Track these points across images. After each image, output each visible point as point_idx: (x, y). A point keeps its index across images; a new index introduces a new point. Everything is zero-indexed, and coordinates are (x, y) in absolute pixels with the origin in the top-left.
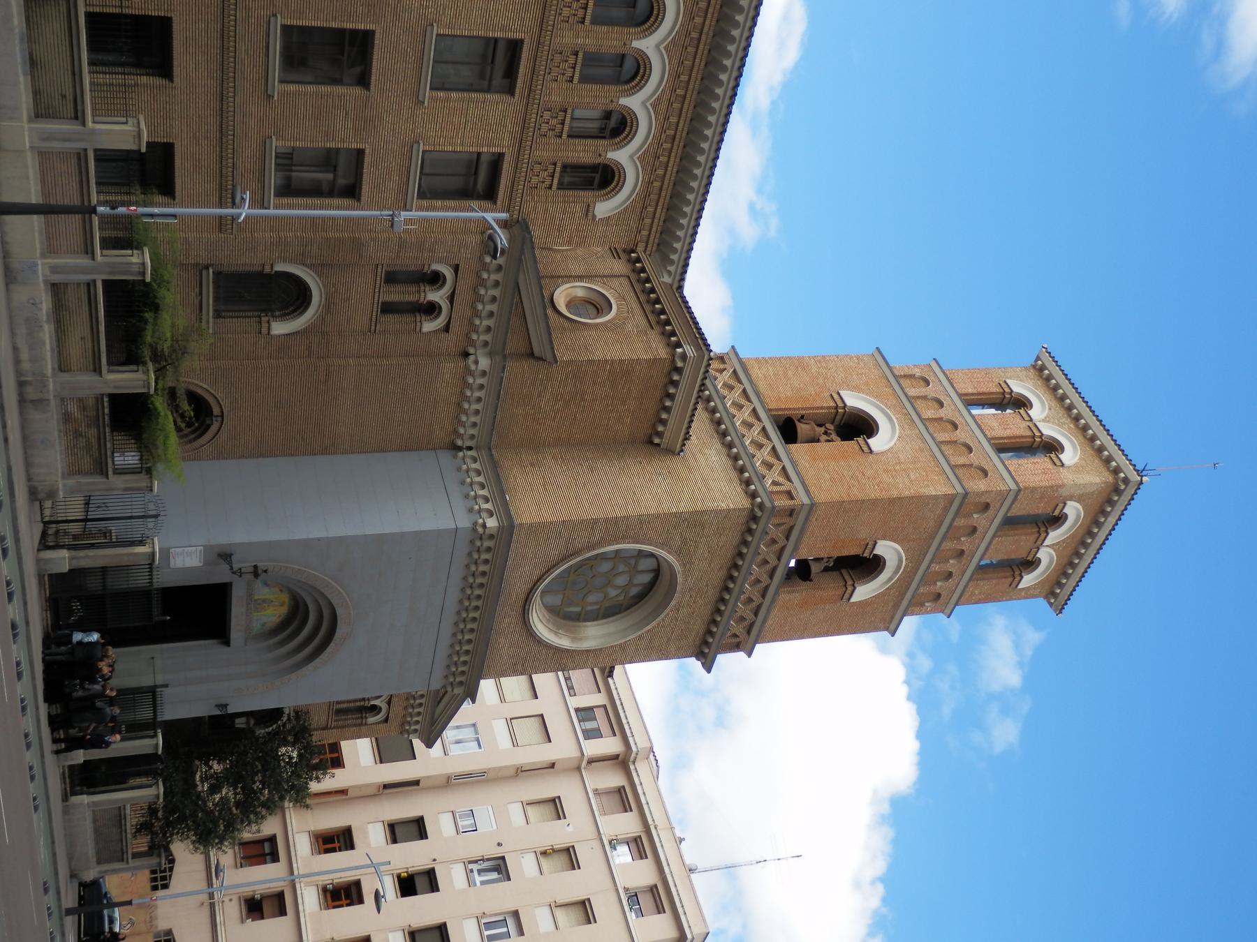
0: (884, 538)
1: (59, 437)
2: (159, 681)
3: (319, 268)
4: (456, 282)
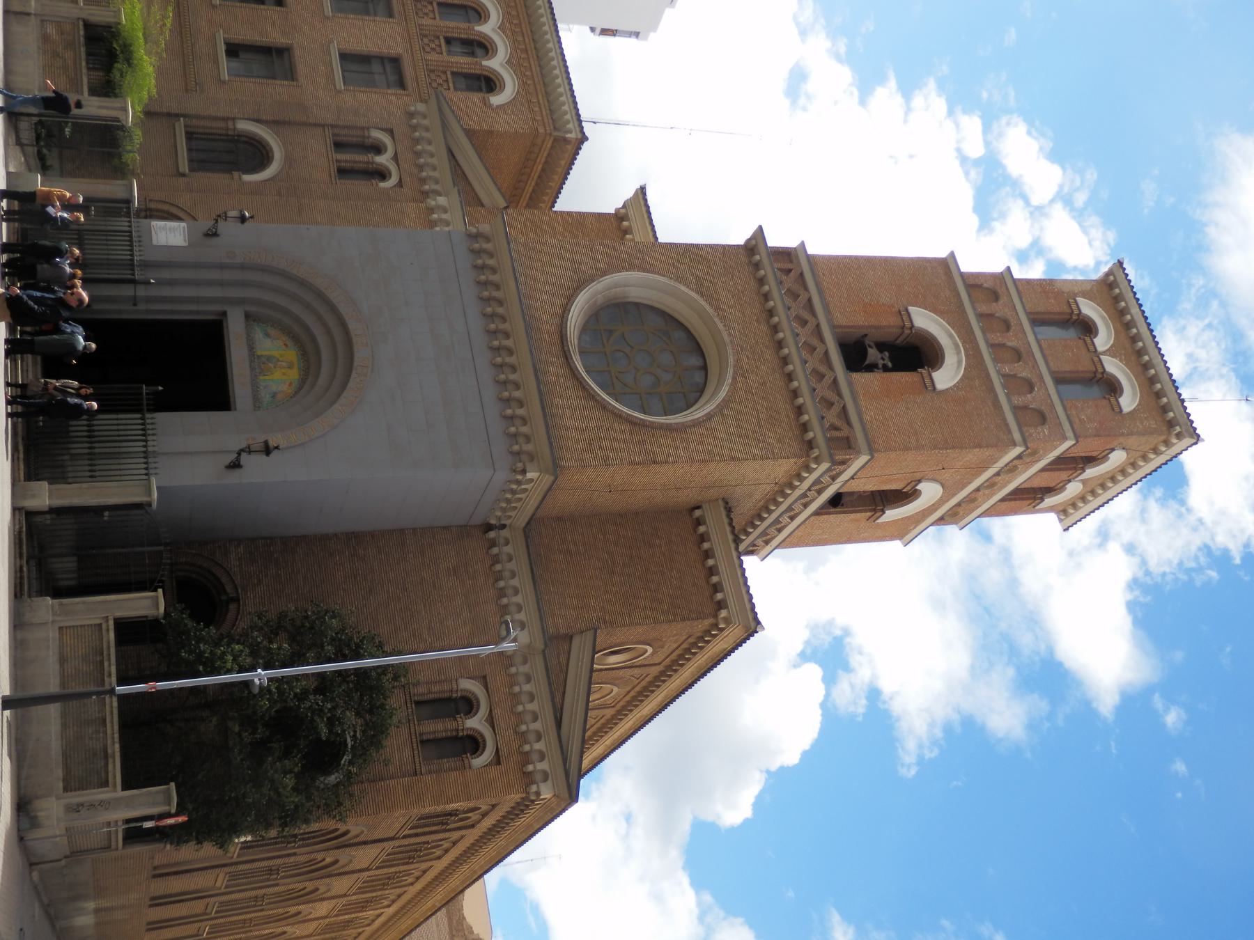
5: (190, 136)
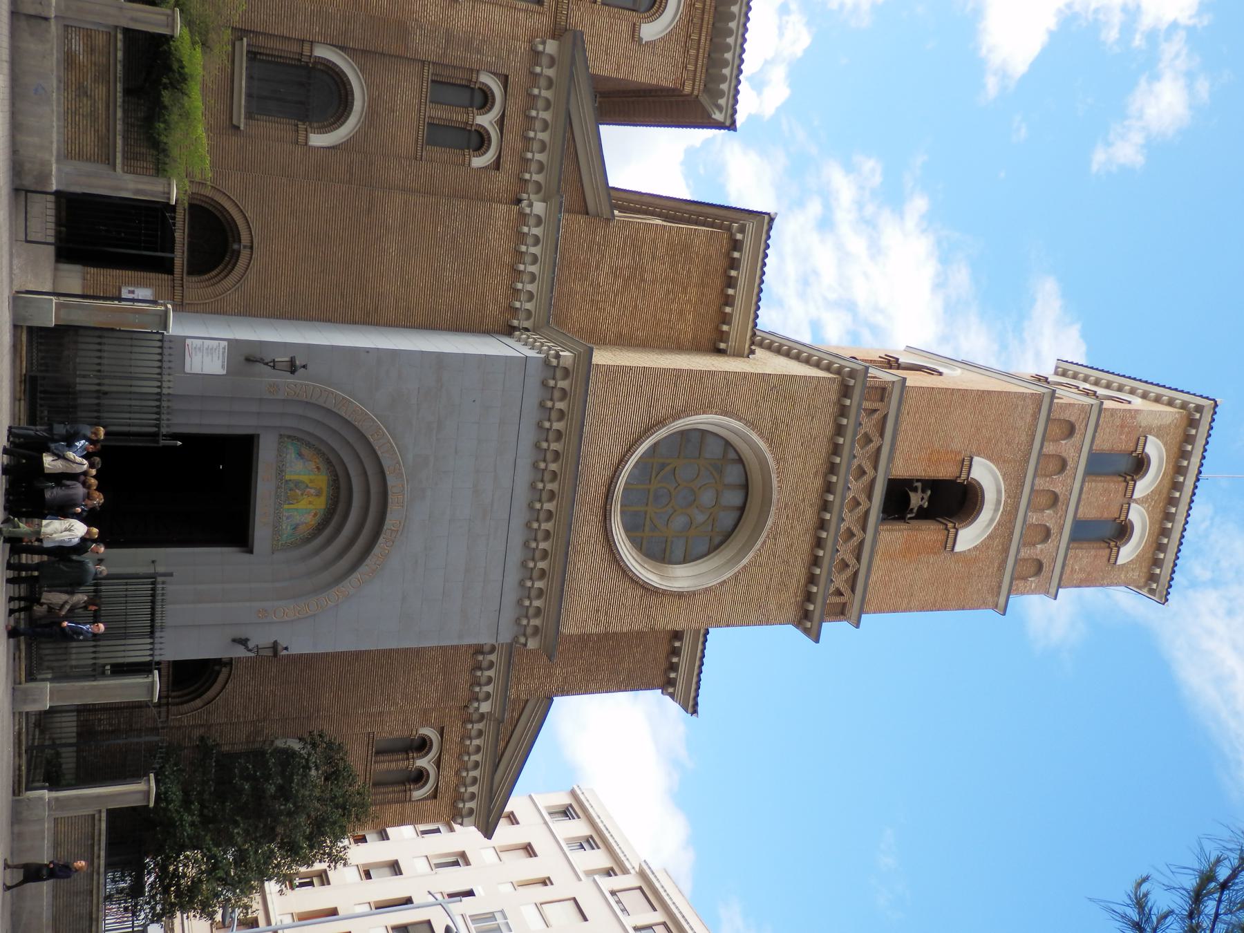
0: (979, 455)
1: (58, 88)
2: (160, 569)
3: (359, 54)
4: (506, 99)
5: (253, 56)
